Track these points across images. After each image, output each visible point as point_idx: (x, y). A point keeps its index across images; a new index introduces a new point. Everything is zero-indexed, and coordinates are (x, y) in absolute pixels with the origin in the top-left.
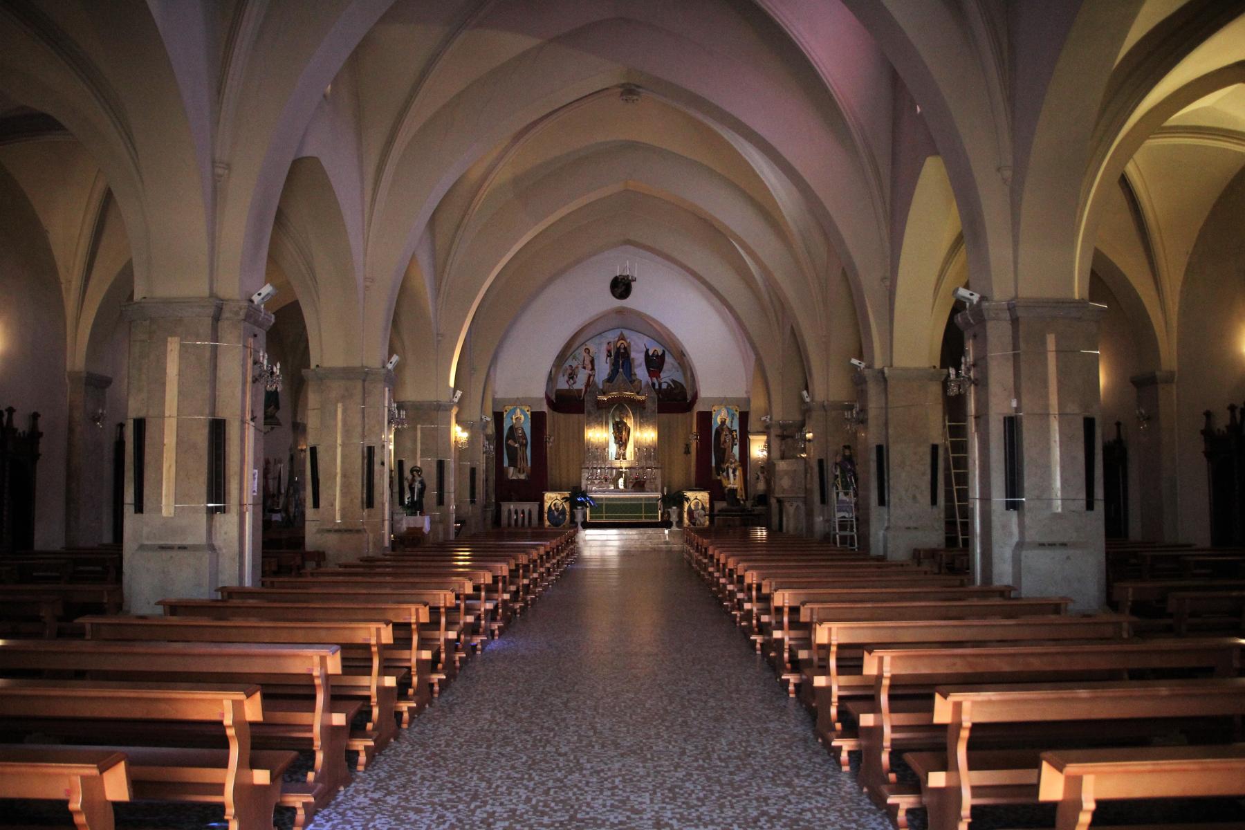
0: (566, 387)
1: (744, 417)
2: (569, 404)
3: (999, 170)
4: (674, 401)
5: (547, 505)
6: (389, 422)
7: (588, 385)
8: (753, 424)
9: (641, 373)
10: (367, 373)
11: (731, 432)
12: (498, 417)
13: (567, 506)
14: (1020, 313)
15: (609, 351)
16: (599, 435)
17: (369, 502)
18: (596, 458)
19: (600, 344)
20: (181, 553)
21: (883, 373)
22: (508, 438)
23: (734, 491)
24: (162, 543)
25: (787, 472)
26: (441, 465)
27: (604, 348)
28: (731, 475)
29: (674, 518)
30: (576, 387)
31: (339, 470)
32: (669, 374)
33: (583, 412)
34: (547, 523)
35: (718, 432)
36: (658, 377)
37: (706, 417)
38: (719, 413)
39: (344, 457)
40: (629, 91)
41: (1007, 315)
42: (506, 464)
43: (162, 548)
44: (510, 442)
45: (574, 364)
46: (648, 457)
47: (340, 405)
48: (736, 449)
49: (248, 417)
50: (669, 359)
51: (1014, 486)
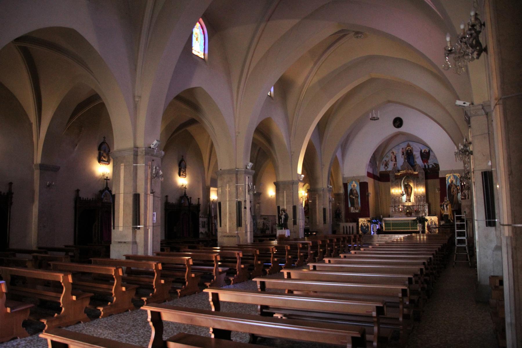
0: (384, 170)
2: (384, 178)
4: (431, 174)
5: (360, 224)
6: (249, 191)
9: (419, 161)
10: (237, 171)
11: (456, 186)
12: (345, 185)
15: (403, 152)
16: (396, 191)
17: (239, 224)
18: (395, 202)
19: (399, 149)
20: (125, 245)
22: (350, 195)
23: (447, 216)
24: (119, 240)
26: (295, 208)
27: (401, 150)
28: (445, 208)
30: (388, 170)
31: (228, 212)
33: (389, 181)
34: (360, 232)
35: (450, 187)
36: (427, 162)
37: (443, 180)
38: (450, 177)
39: (229, 206)
40: (341, 35)
42: (350, 206)
43: (120, 242)
44: (351, 196)
45: (387, 159)
46: (420, 201)
47: (228, 185)
49: (149, 192)
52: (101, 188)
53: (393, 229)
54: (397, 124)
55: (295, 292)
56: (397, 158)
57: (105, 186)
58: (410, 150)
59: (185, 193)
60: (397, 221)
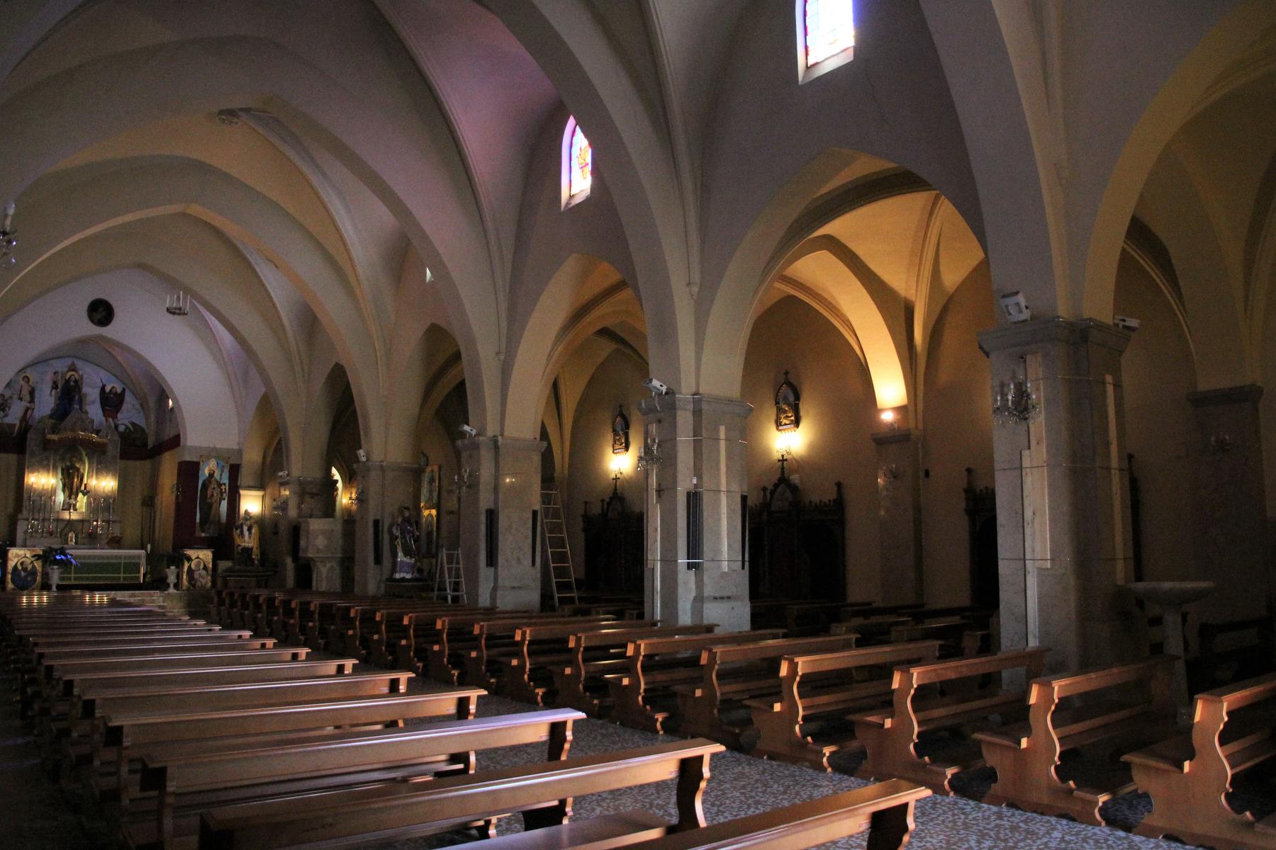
1: (235, 470)
3: (689, 284)
5: (11, 564)
7: (24, 419)
8: (245, 476)
9: (94, 411)
11: (220, 485)
13: (38, 565)
14: (705, 406)
16: (42, 480)
21: (496, 442)
23: (248, 551)
25: (323, 532)
27: (49, 378)
28: (246, 533)
29: (172, 579)
32: (129, 414)
35: (205, 486)
36: (115, 417)
37: (189, 471)
41: (691, 407)
48: (224, 504)
50: (128, 397)
51: (694, 549)
52: (775, 479)
53: (76, 579)
54: (98, 316)
55: (379, 727)
56: (37, 394)
57: (778, 475)
58: (76, 381)
59: (616, 489)
60: (89, 557)
